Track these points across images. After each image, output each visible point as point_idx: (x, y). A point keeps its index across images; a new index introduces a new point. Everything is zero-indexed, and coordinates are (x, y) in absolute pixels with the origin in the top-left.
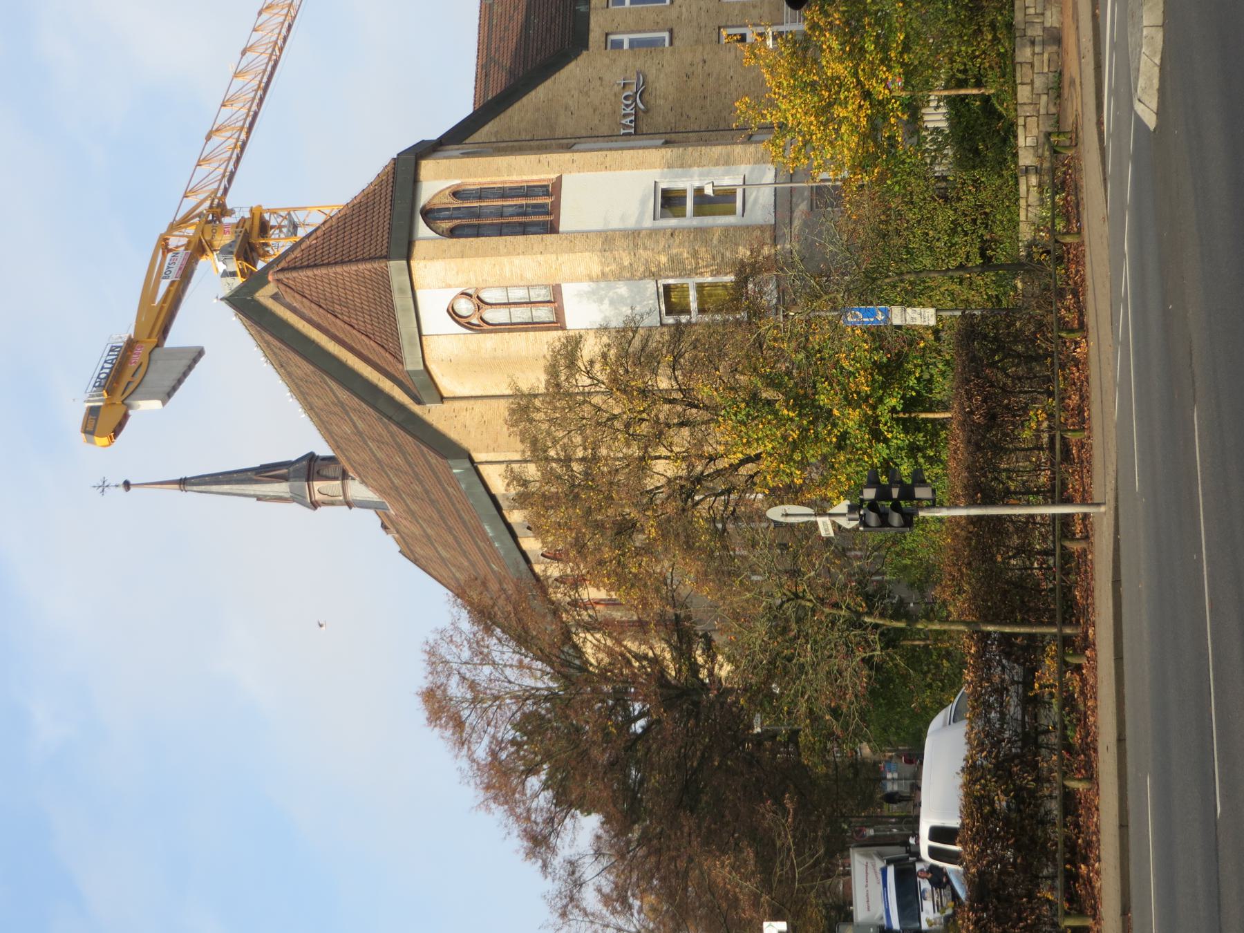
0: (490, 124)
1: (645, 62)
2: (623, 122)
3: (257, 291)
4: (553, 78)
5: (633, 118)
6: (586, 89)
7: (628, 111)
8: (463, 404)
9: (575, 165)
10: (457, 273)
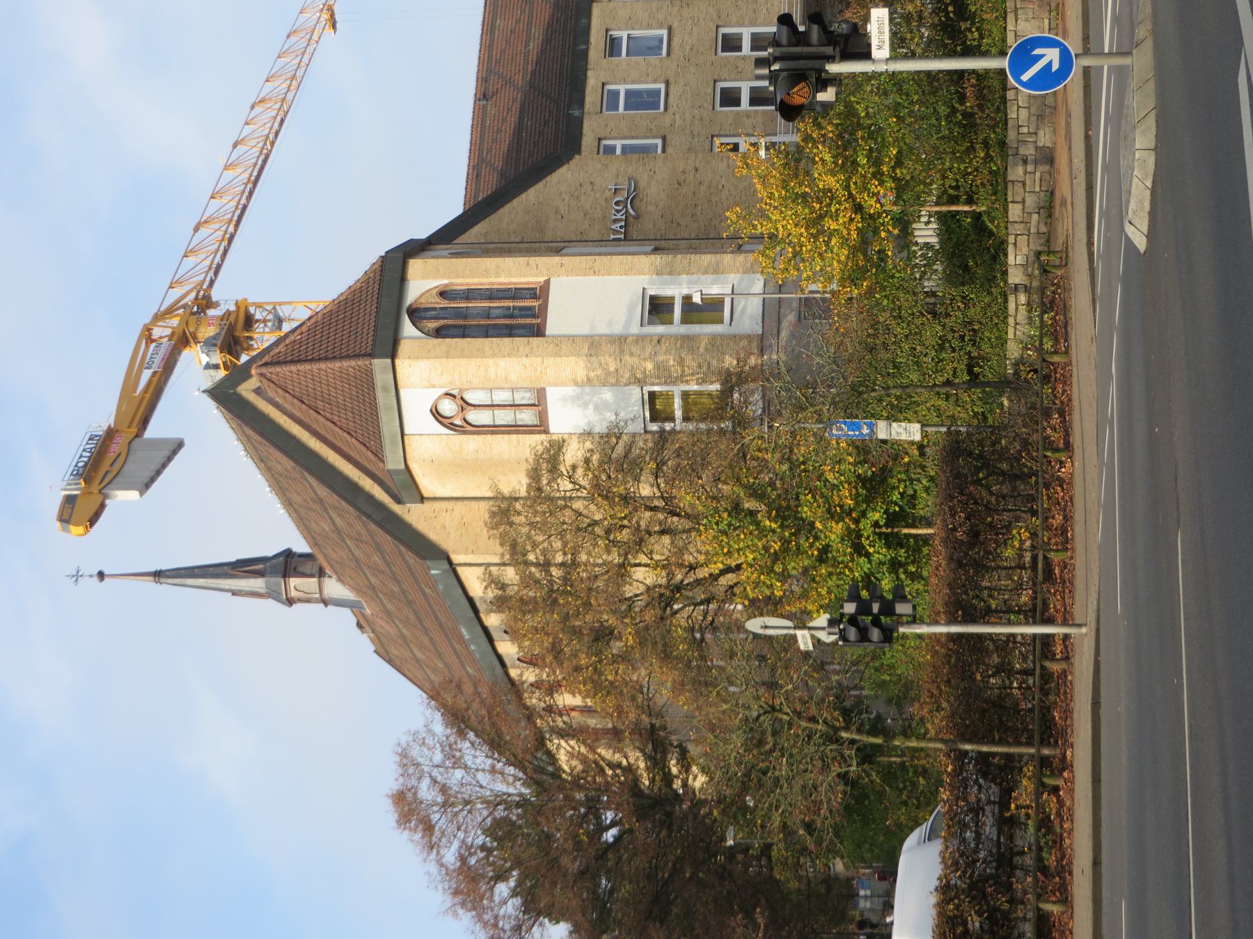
0: (480, 225)
2: (613, 227)
4: (544, 181)
5: (623, 223)
7: (619, 216)
8: (443, 505)
9: (563, 268)
10: (442, 374)
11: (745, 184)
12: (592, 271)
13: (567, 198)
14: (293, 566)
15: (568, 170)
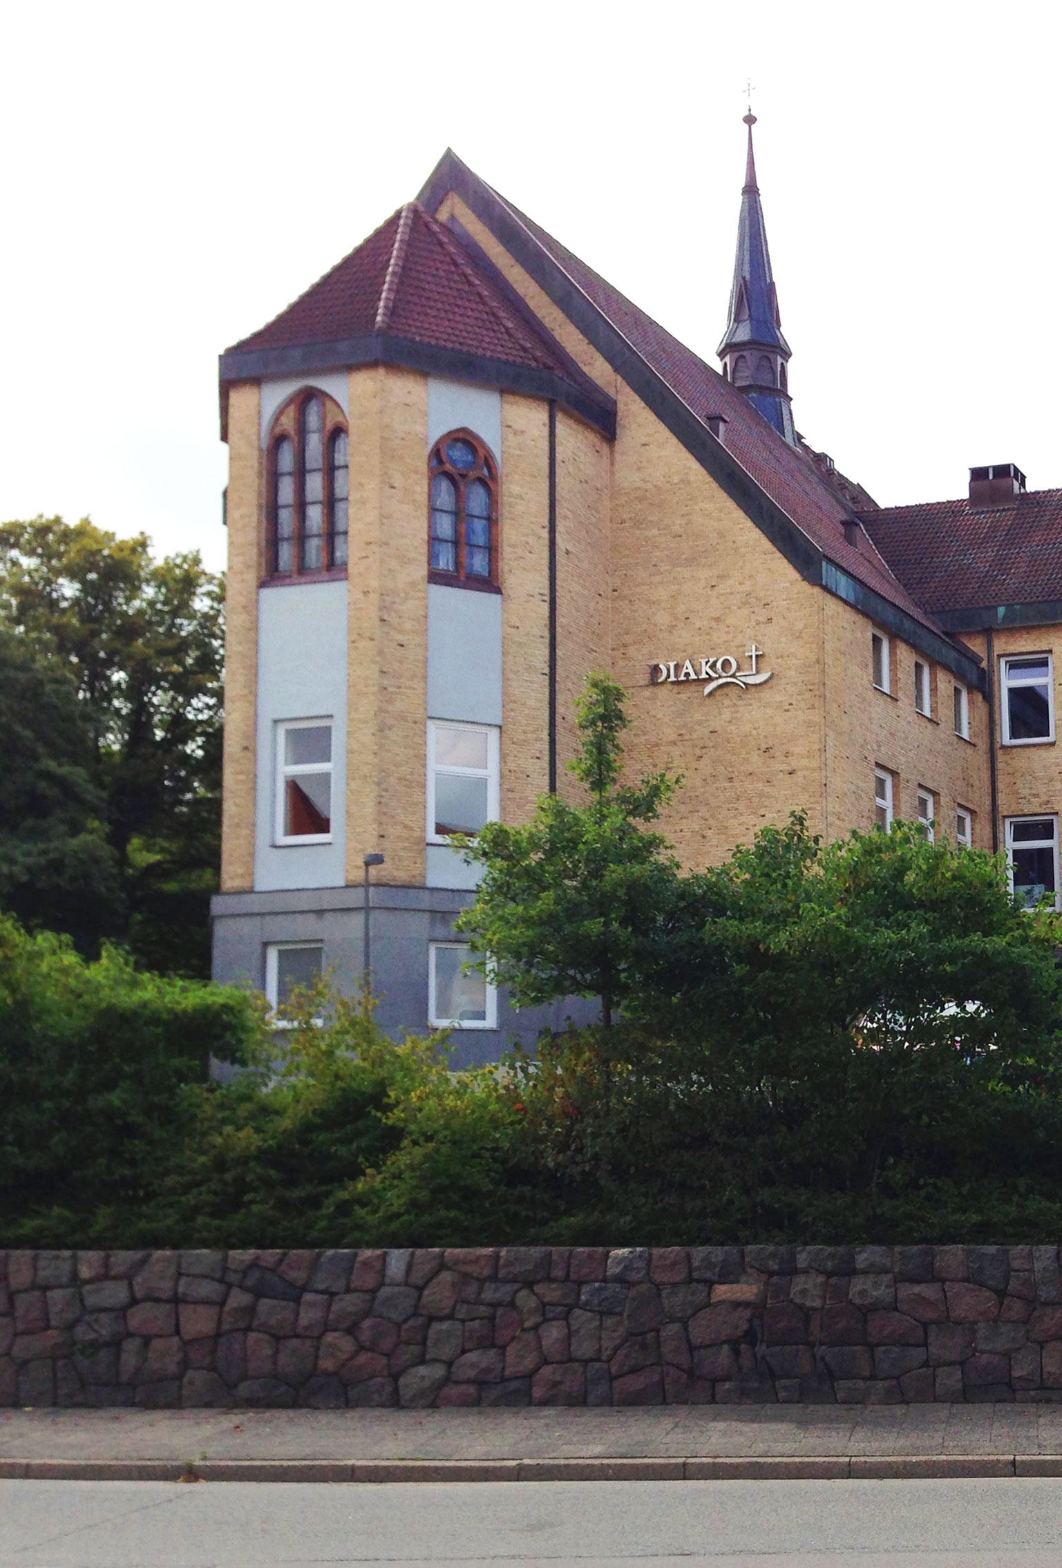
0: (702, 471)
3: (460, 195)
5: (693, 676)
9: (361, 595)
13: (746, 588)
14: (745, 353)
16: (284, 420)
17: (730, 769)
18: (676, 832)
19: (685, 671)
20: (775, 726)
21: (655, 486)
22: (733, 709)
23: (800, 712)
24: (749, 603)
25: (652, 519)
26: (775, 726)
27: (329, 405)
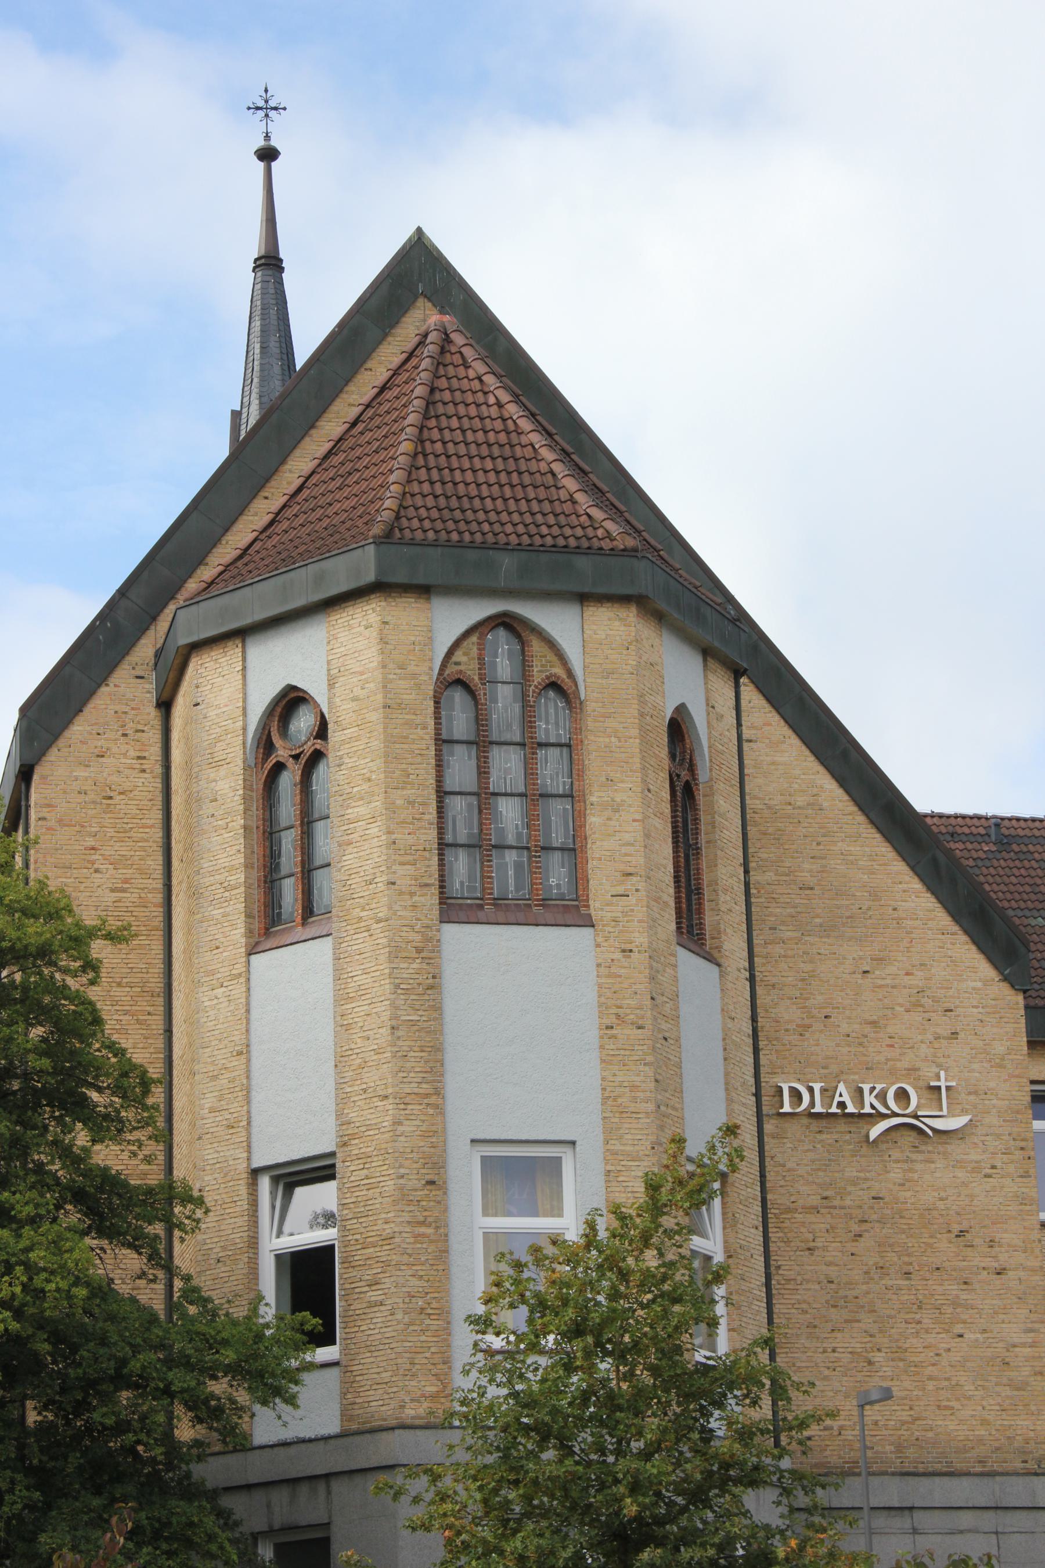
0: (840, 792)
1: (998, 1136)
2: (841, 1088)
4: (956, 928)
5: (851, 1109)
6: (927, 1002)
7: (869, 1099)
8: (155, 751)
9: (618, 955)
10: (355, 699)
11: (969, 1387)
12: (613, 1020)
13: (917, 980)
15: (986, 982)
16: (459, 656)
17: (906, 1259)
18: (824, 1352)
19: (837, 1099)
20: (972, 1197)
21: (769, 808)
22: (905, 1166)
23: (1008, 1181)
24: (922, 1006)
25: (764, 856)
26: (972, 1197)
27: (536, 646)
